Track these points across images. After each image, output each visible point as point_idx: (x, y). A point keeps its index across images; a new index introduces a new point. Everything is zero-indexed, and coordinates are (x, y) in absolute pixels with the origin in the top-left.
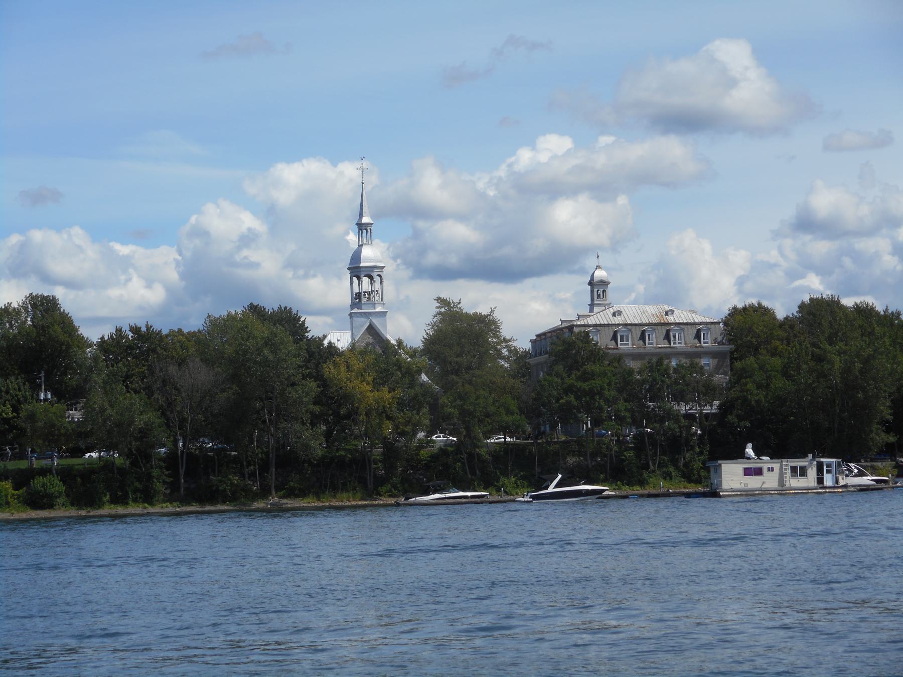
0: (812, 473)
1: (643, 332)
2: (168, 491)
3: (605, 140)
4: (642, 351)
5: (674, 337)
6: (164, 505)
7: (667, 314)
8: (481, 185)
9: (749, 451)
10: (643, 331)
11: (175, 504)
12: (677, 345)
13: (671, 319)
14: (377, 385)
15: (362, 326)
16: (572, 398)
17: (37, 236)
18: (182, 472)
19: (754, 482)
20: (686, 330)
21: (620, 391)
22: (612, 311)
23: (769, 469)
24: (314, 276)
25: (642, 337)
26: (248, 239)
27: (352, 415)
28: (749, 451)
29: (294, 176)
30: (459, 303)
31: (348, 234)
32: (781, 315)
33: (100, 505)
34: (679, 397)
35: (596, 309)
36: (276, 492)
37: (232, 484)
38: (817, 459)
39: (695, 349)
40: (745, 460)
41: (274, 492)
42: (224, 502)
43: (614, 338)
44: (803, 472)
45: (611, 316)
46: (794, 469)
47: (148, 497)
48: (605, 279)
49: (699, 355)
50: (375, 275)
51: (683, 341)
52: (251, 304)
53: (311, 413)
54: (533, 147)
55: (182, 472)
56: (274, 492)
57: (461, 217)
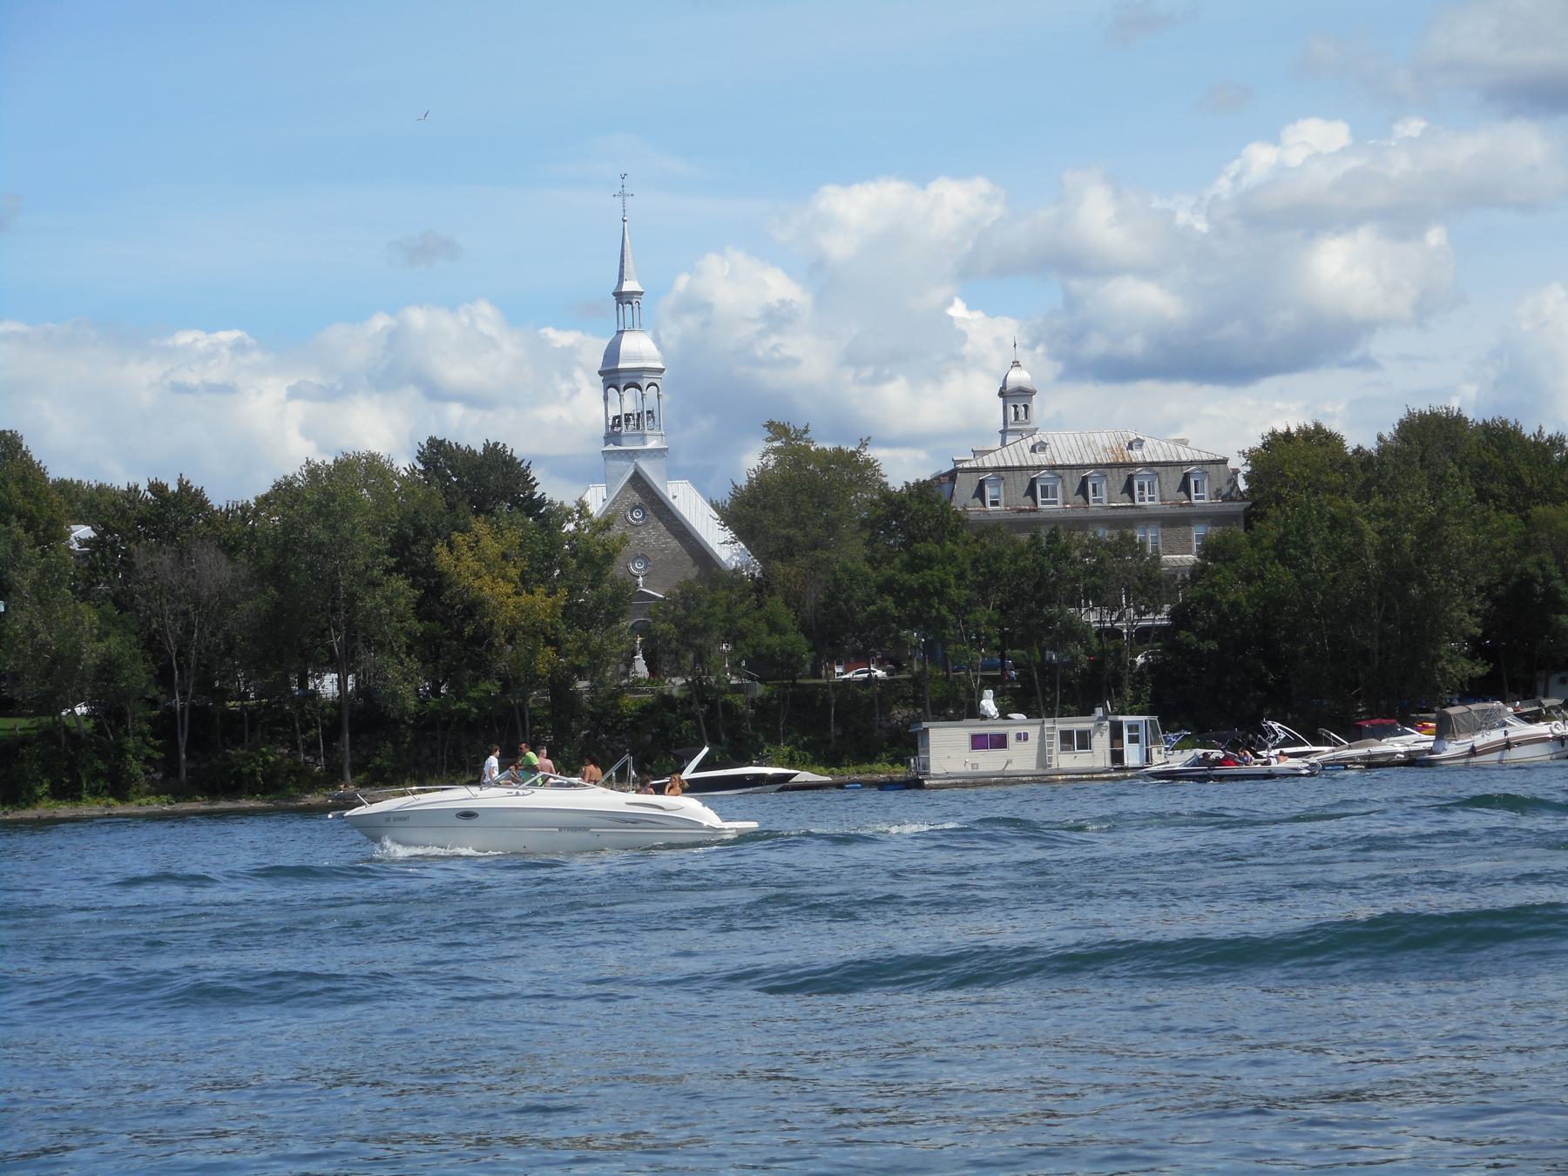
0: (1101, 742)
1: (1084, 480)
2: (159, 776)
3: (1414, 127)
4: (1081, 513)
5: (1141, 487)
6: (143, 801)
7: (1130, 447)
8: (1182, 218)
9: (989, 704)
10: (1082, 478)
11: (164, 798)
12: (1147, 503)
13: (1137, 455)
14: (524, 584)
15: (622, 475)
16: (888, 602)
17: (417, 318)
18: (182, 741)
19: (990, 762)
20: (1163, 475)
21: (982, 588)
22: (1031, 442)
23: (1019, 737)
24: (891, 378)
25: (1083, 490)
26: (777, 318)
27: (482, 638)
28: (989, 704)
29: (857, 209)
30: (806, 431)
31: (950, 303)
32: (1351, 444)
33: (32, 801)
34: (1097, 596)
35: (1010, 439)
36: (353, 775)
37: (266, 762)
38: (1111, 718)
39: (1182, 510)
40: (977, 721)
41: (348, 776)
42: (252, 794)
43: (1031, 491)
44: (1084, 741)
45: (1027, 452)
46: (1066, 737)
47: (119, 788)
48: (1025, 386)
49: (1130, 522)
50: (644, 383)
51: (1157, 495)
52: (431, 439)
53: (409, 634)
54: (1274, 139)
55: (182, 741)
56: (348, 776)
57: (1147, 272)
